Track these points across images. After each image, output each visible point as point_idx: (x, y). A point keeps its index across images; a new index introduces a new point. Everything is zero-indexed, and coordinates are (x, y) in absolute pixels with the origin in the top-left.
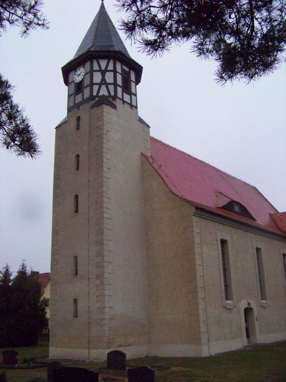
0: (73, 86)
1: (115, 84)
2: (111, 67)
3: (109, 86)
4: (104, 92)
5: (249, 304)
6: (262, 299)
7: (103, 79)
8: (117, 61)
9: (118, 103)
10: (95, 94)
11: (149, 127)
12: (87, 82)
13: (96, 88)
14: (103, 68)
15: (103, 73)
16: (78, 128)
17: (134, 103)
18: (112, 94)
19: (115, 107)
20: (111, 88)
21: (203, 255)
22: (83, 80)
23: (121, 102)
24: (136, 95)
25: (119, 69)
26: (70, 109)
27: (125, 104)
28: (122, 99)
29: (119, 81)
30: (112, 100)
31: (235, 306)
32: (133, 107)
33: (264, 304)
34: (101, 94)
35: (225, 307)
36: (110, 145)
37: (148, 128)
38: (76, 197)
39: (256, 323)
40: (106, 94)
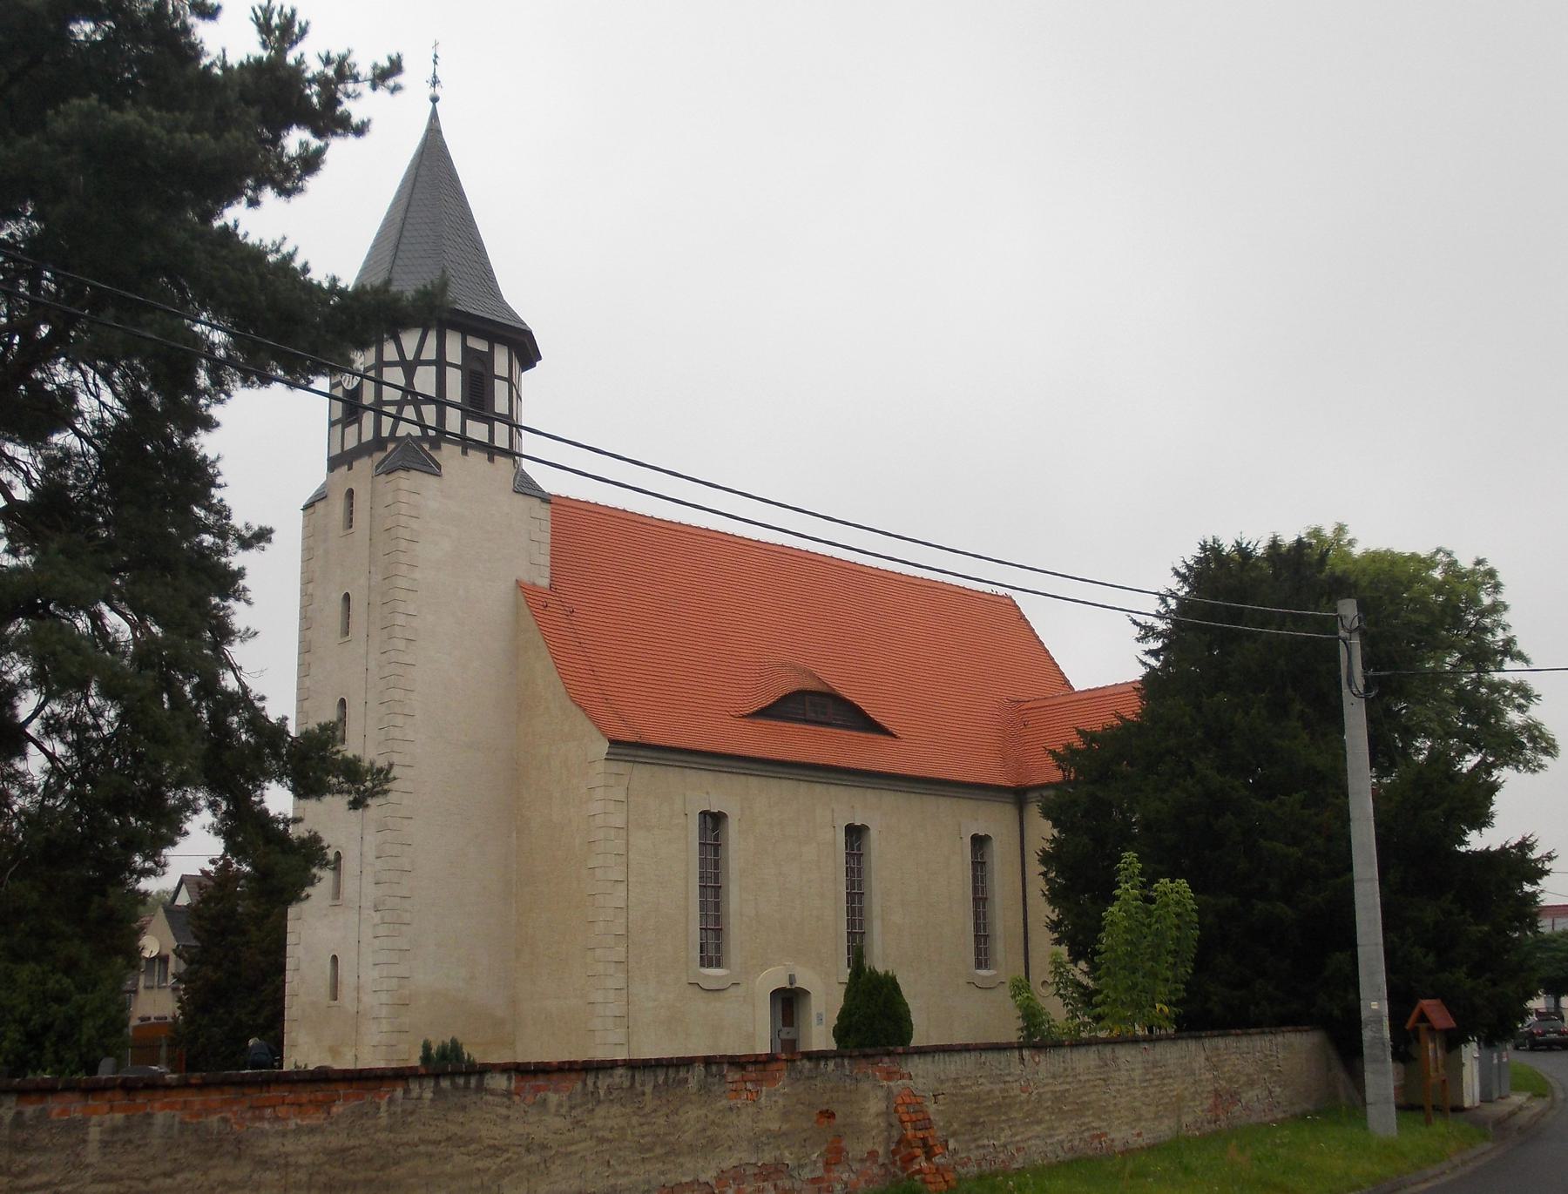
1: (441, 402)
2: (430, 352)
14: (410, 356)
20: (430, 413)
21: (631, 856)
25: (454, 352)
26: (334, 463)
29: (454, 391)
30: (431, 448)
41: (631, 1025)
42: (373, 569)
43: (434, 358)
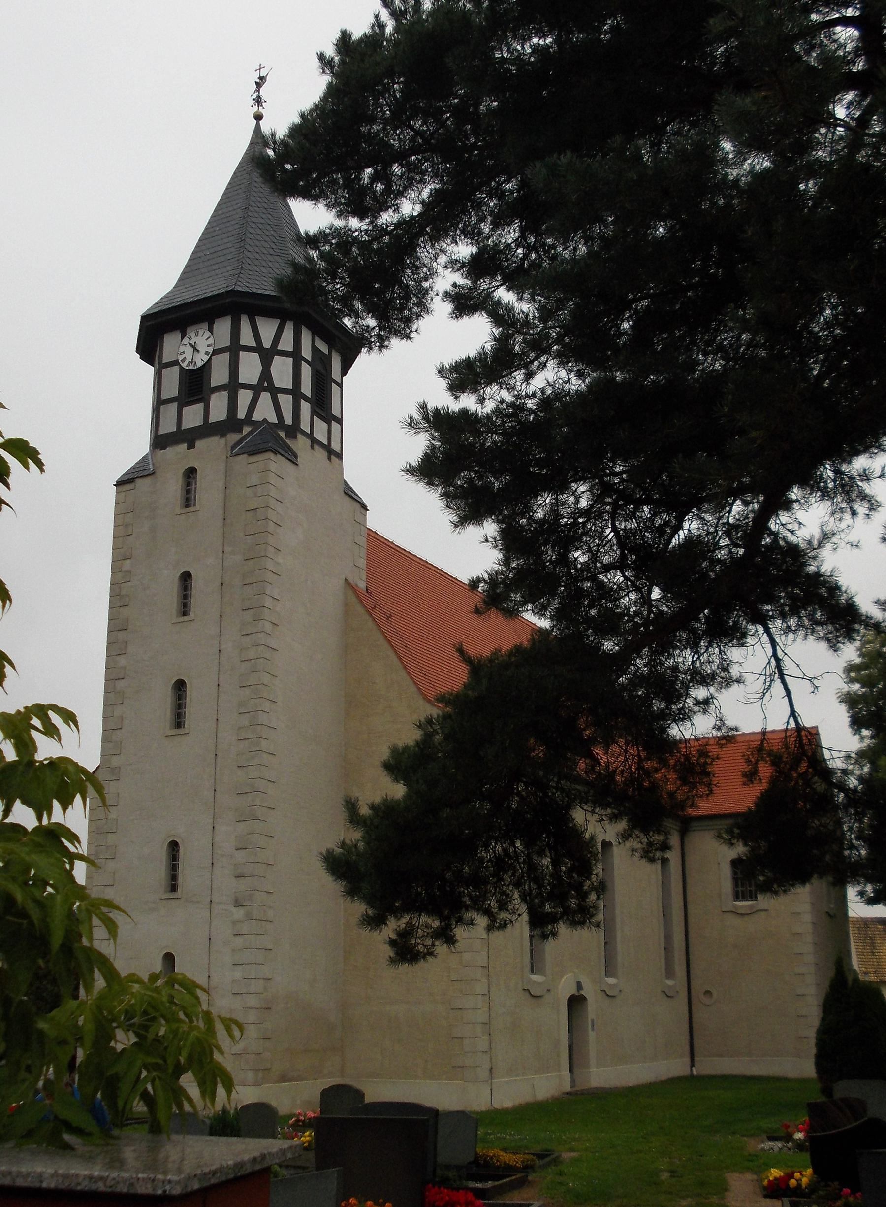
0: (172, 377)
3: (281, 397)
4: (265, 411)
5: (579, 986)
6: (532, 972)
7: (266, 375)
8: (303, 326)
9: (300, 444)
10: (241, 414)
11: (364, 507)
12: (219, 376)
13: (244, 397)
14: (267, 344)
15: (267, 356)
16: (188, 500)
17: (335, 446)
18: (288, 420)
19: (292, 457)
20: (286, 401)
22: (208, 365)
23: (308, 442)
24: (340, 421)
25: (306, 352)
26: (159, 441)
27: (316, 447)
28: (310, 436)
29: (306, 388)
31: (549, 990)
32: (333, 457)
33: (612, 986)
34: (257, 417)
35: (605, 991)
36: (281, 561)
37: (363, 511)
38: (180, 686)
39: (592, 1035)
40: (273, 419)
41: (491, 1032)
42: (228, 549)
43: (292, 350)
